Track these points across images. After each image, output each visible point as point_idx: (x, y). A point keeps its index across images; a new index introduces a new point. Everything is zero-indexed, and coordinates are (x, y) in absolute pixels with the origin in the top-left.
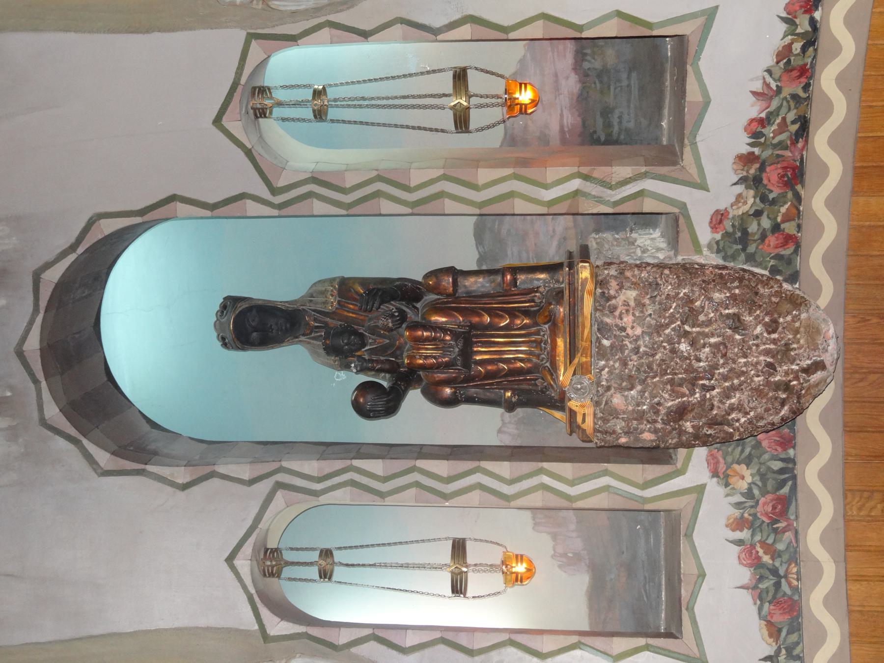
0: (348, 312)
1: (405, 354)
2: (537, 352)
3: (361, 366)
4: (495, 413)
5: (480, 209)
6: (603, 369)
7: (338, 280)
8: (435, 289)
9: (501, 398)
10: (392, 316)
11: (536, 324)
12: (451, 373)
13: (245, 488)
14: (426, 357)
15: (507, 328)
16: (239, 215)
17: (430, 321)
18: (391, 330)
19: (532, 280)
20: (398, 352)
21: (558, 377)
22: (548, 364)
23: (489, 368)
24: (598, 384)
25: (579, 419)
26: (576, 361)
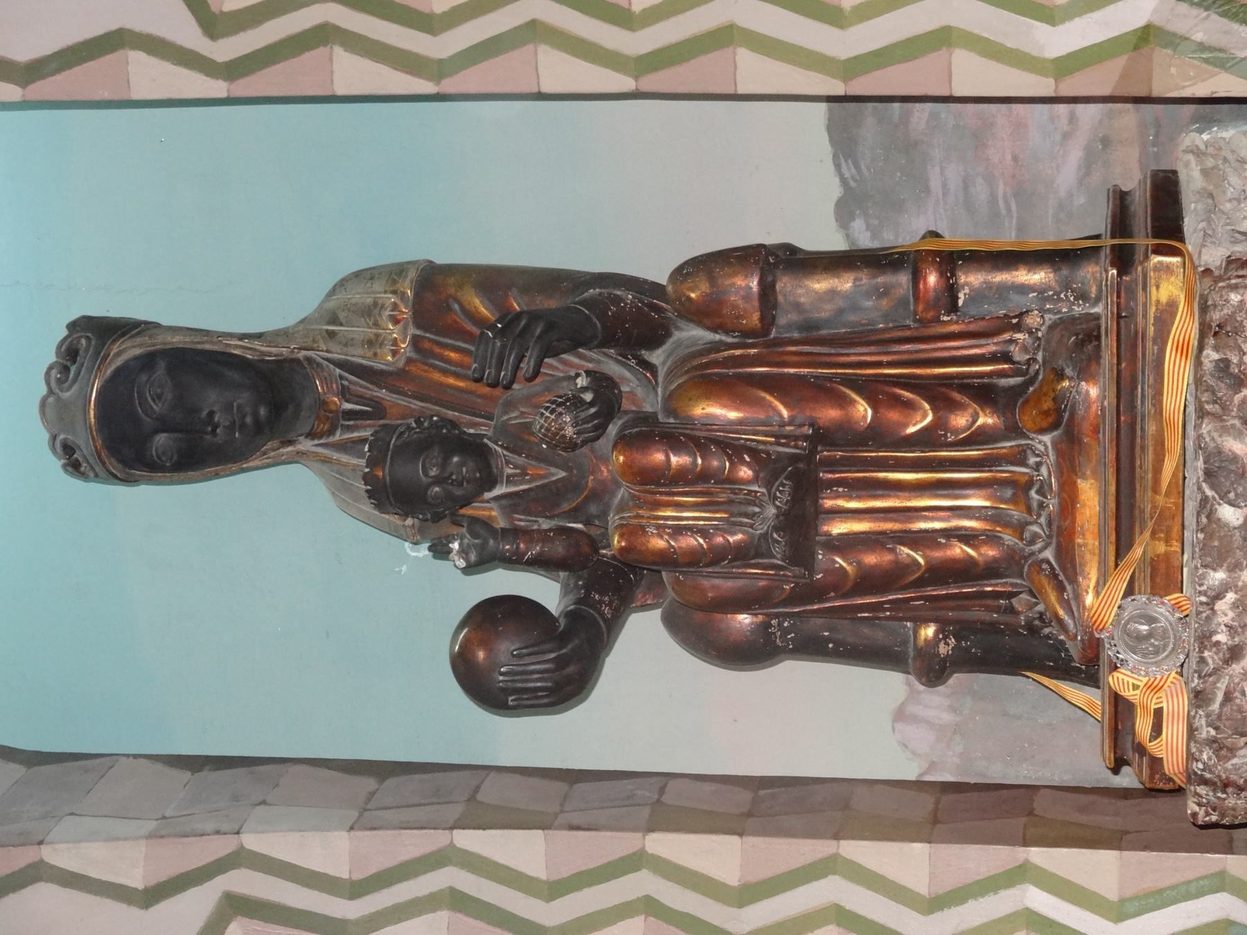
0: (445, 372)
1: (613, 519)
2: (1016, 514)
3: (482, 548)
4: (888, 686)
5: (846, 80)
6: (1219, 596)
7: (412, 274)
8: (707, 314)
9: (905, 643)
10: (575, 403)
11: (1013, 430)
12: (755, 576)
13: (135, 912)
14: (678, 531)
15: (927, 438)
16: (106, 95)
17: (690, 421)
18: (572, 446)
19: (1003, 289)
20: (593, 509)
21: (1078, 598)
22: (1049, 554)
23: (871, 559)
24: (1204, 639)
25: (1143, 726)
26: (1137, 551)
